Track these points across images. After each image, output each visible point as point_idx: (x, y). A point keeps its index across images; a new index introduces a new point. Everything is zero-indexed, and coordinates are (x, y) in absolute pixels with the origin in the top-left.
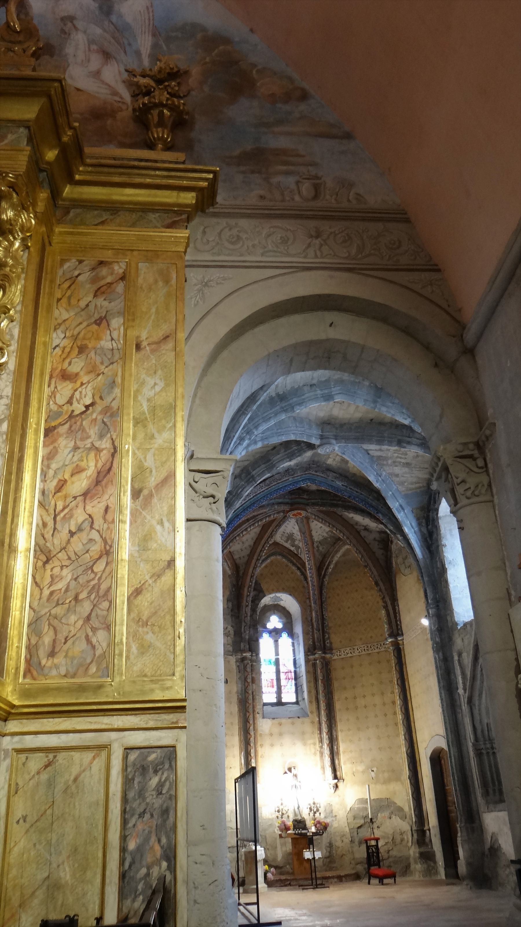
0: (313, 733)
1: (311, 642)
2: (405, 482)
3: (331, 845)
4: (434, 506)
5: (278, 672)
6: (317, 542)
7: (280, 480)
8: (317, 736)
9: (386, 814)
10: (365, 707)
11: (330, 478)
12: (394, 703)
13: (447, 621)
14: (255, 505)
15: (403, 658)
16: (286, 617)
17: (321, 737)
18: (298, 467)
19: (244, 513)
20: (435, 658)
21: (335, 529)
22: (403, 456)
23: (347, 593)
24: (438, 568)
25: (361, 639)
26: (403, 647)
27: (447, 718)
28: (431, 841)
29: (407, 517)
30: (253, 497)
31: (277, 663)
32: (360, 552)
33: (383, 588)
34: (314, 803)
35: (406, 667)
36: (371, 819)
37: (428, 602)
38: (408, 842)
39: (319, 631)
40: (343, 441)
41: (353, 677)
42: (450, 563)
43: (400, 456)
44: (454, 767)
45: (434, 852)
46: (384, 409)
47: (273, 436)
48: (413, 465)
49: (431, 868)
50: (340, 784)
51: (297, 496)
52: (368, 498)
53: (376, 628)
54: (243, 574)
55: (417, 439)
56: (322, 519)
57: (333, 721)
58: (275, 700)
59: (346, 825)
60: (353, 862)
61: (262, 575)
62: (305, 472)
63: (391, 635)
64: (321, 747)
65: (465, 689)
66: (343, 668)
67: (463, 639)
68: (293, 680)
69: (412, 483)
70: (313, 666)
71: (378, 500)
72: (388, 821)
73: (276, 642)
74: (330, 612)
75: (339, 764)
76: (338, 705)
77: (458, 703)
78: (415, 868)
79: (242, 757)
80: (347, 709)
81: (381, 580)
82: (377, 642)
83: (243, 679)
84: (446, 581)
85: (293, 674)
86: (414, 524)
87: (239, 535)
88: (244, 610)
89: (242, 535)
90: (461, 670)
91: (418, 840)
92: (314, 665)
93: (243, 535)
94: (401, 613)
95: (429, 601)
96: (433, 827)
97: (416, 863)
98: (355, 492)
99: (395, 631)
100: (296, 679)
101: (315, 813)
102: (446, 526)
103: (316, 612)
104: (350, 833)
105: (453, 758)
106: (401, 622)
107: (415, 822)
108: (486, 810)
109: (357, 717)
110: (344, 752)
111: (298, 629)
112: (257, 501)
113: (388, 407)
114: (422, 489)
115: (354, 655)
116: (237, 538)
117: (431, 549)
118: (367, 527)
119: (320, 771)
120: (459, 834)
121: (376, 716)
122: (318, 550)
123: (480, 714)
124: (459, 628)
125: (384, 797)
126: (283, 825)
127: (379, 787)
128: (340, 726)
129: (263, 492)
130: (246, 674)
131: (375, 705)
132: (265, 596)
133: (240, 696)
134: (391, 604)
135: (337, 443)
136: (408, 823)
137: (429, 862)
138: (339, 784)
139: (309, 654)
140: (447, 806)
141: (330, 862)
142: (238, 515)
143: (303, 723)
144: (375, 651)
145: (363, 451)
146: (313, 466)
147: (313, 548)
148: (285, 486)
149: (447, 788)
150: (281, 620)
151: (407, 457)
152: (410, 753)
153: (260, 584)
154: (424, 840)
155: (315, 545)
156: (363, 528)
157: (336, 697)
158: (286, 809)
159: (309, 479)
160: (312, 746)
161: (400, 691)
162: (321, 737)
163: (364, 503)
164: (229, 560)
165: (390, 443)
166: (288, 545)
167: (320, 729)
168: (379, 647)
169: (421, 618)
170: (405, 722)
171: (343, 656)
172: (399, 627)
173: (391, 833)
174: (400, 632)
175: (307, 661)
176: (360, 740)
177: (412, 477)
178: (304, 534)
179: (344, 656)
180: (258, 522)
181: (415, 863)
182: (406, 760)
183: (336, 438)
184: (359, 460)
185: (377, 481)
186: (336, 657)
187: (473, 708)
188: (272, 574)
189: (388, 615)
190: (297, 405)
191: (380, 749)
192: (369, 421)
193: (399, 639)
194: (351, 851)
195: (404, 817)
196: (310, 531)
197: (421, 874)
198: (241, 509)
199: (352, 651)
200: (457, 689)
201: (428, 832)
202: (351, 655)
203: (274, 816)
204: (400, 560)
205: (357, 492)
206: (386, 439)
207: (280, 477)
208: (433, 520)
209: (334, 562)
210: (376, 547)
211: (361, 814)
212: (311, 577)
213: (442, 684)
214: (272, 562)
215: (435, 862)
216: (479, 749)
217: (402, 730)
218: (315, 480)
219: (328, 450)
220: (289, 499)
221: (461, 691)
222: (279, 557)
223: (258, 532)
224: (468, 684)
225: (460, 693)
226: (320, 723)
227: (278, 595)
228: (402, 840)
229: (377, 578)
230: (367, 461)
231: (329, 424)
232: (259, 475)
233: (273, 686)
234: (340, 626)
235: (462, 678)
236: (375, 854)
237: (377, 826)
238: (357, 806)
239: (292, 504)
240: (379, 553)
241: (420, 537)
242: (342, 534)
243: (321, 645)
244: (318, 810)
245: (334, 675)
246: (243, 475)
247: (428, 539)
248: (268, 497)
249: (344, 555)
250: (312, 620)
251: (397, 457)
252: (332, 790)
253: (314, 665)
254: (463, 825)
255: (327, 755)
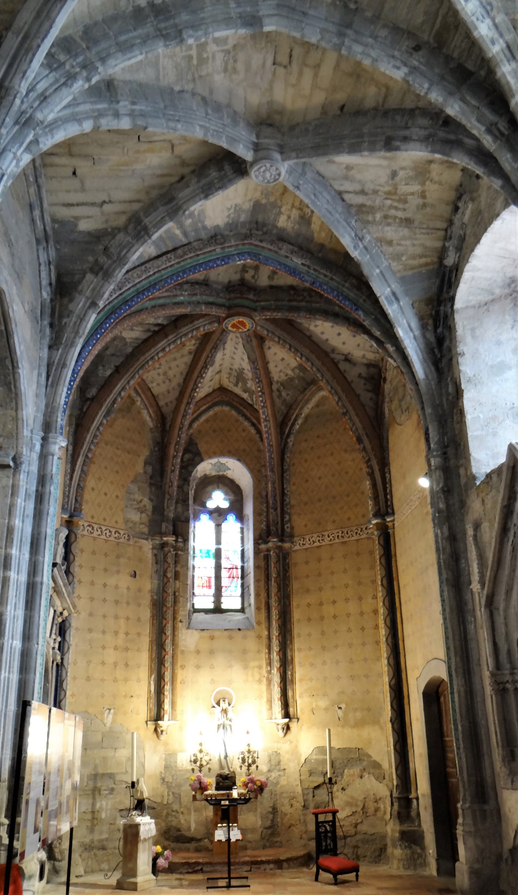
0: (259, 652)
1: (263, 526)
2: (402, 255)
3: (274, 810)
4: (448, 293)
5: (218, 568)
6: (278, 382)
7: (201, 250)
8: (264, 656)
9: (356, 770)
10: (335, 617)
11: (283, 252)
12: (376, 612)
13: (459, 476)
14: (157, 287)
15: (392, 547)
16: (234, 492)
17: (270, 658)
18: (232, 234)
19: (138, 298)
20: (436, 536)
21: (299, 355)
22: (401, 206)
23: (319, 457)
24: (448, 394)
25: (334, 522)
26: (394, 532)
27: (450, 630)
28: (418, 815)
29: (403, 313)
30: (154, 274)
31: (218, 554)
32: (336, 393)
33: (368, 446)
34: (249, 752)
35: (396, 561)
36: (330, 779)
37: (429, 448)
38: (385, 813)
39: (276, 510)
40: (294, 154)
41: (320, 575)
42: (469, 381)
43: (395, 204)
44: (457, 710)
45: (423, 832)
46: (358, 48)
47: (158, 117)
48: (416, 224)
49: (416, 856)
50: (293, 725)
51: (239, 295)
52: (343, 286)
53: (356, 505)
54: (170, 426)
55: (421, 128)
56: (279, 338)
57: (288, 636)
58: (211, 606)
59: (299, 783)
60: (304, 836)
61: (200, 431)
62: (243, 240)
63: (376, 515)
64: (270, 672)
65: (482, 583)
66: (307, 563)
67: (483, 501)
68: (240, 579)
69: (414, 257)
70: (264, 559)
71: (359, 289)
72: (358, 780)
73: (218, 526)
74: (294, 484)
75: (293, 696)
76: (296, 614)
77: (470, 606)
78: (393, 853)
79: (152, 682)
80: (309, 620)
81: (367, 435)
82: (357, 525)
83: (162, 573)
84: (461, 413)
85: (239, 571)
86: (414, 323)
87: (152, 358)
88: (168, 477)
89: (156, 358)
90: (477, 552)
91: (399, 813)
92: (267, 558)
93: (159, 358)
94: (393, 482)
95: (432, 445)
96: (423, 795)
97: (394, 846)
98: (322, 277)
99: (383, 510)
100: (243, 577)
101: (249, 765)
102: (465, 323)
103: (273, 483)
104: (304, 795)
105: (456, 695)
106: (392, 496)
107: (397, 786)
108: (509, 785)
109: (323, 631)
110: (301, 680)
111: (249, 509)
112: (161, 281)
113: (366, 45)
114: (431, 267)
115: (324, 543)
116: (150, 363)
117: (440, 366)
118: (349, 357)
119: (265, 706)
120: (460, 820)
121: (349, 630)
122: (280, 396)
123: (506, 625)
124: (478, 483)
125: (354, 747)
126: (197, 782)
127: (348, 731)
128: (297, 643)
129: (171, 266)
130: (166, 565)
131: (348, 615)
132: (202, 460)
133: (155, 597)
134: (379, 470)
135: (283, 160)
136: (387, 786)
137: (414, 846)
138: (291, 725)
139: (260, 541)
140: (445, 766)
141: (273, 834)
142: (127, 301)
143: (245, 637)
144: (353, 538)
145: (333, 193)
146: (256, 232)
147: (272, 391)
148: (210, 261)
149: (447, 739)
150: (227, 497)
151: (406, 206)
152: (395, 685)
153: (196, 444)
154: (409, 813)
155: (275, 387)
156: (343, 357)
157: (295, 602)
158: (207, 758)
159: (249, 253)
160: (256, 670)
161: (385, 594)
162: (270, 658)
163: (335, 293)
164: (152, 406)
165: (372, 149)
166: (238, 390)
167: (269, 648)
168: (359, 532)
169: (418, 477)
170: (390, 640)
171: (307, 546)
172: (389, 503)
173: (361, 798)
174: (390, 510)
175: (257, 552)
176: (324, 663)
177: (414, 245)
178: (253, 363)
179: (309, 546)
180: (181, 337)
181: (393, 847)
182: (389, 695)
183: (282, 149)
184: (325, 206)
185: (355, 247)
186: (297, 547)
187: (495, 613)
188: (214, 431)
189: (374, 485)
190: (187, 27)
191: (352, 677)
192: (339, 112)
193: (388, 520)
194: (302, 821)
195: (381, 778)
196: (266, 363)
197: (402, 863)
198: (133, 292)
199: (320, 539)
200: (470, 583)
201: (415, 801)
202: (320, 544)
203: (190, 767)
204: (396, 403)
205: (325, 276)
206: (366, 139)
207: (201, 246)
208: (446, 317)
209: (303, 415)
210: (360, 387)
211: (321, 769)
212: (267, 432)
213: (445, 576)
214: (216, 414)
215: (423, 848)
216: (502, 683)
217: (384, 651)
218: (259, 255)
219: (268, 175)
220: (225, 298)
221: (475, 586)
222: (226, 409)
223: (189, 363)
224: (488, 573)
225: (475, 590)
226: (269, 638)
227: (223, 460)
228: (377, 810)
229: (361, 431)
230: (340, 209)
231: (271, 125)
232: (154, 226)
233: (210, 587)
234: (306, 504)
235: (478, 564)
236: (329, 835)
237: (341, 786)
238: (314, 757)
239: (229, 308)
240: (366, 397)
241: (422, 346)
242: (309, 364)
243: (277, 529)
244: (254, 762)
245: (294, 572)
246: (131, 227)
247: (436, 351)
248: (179, 276)
249: (317, 405)
250: (267, 496)
251: (391, 207)
252: (281, 734)
253: (267, 558)
254: (467, 805)
255: (276, 686)
